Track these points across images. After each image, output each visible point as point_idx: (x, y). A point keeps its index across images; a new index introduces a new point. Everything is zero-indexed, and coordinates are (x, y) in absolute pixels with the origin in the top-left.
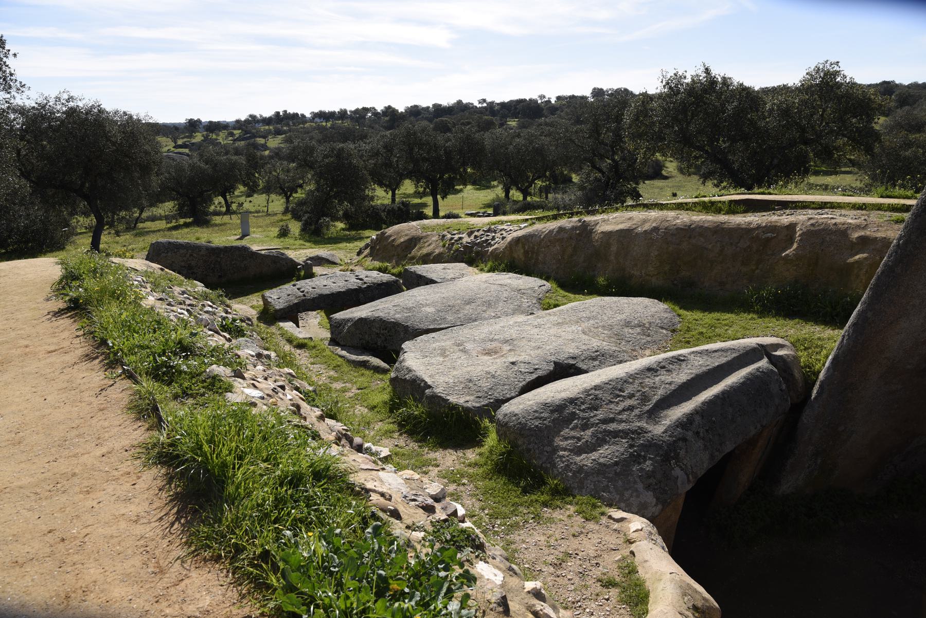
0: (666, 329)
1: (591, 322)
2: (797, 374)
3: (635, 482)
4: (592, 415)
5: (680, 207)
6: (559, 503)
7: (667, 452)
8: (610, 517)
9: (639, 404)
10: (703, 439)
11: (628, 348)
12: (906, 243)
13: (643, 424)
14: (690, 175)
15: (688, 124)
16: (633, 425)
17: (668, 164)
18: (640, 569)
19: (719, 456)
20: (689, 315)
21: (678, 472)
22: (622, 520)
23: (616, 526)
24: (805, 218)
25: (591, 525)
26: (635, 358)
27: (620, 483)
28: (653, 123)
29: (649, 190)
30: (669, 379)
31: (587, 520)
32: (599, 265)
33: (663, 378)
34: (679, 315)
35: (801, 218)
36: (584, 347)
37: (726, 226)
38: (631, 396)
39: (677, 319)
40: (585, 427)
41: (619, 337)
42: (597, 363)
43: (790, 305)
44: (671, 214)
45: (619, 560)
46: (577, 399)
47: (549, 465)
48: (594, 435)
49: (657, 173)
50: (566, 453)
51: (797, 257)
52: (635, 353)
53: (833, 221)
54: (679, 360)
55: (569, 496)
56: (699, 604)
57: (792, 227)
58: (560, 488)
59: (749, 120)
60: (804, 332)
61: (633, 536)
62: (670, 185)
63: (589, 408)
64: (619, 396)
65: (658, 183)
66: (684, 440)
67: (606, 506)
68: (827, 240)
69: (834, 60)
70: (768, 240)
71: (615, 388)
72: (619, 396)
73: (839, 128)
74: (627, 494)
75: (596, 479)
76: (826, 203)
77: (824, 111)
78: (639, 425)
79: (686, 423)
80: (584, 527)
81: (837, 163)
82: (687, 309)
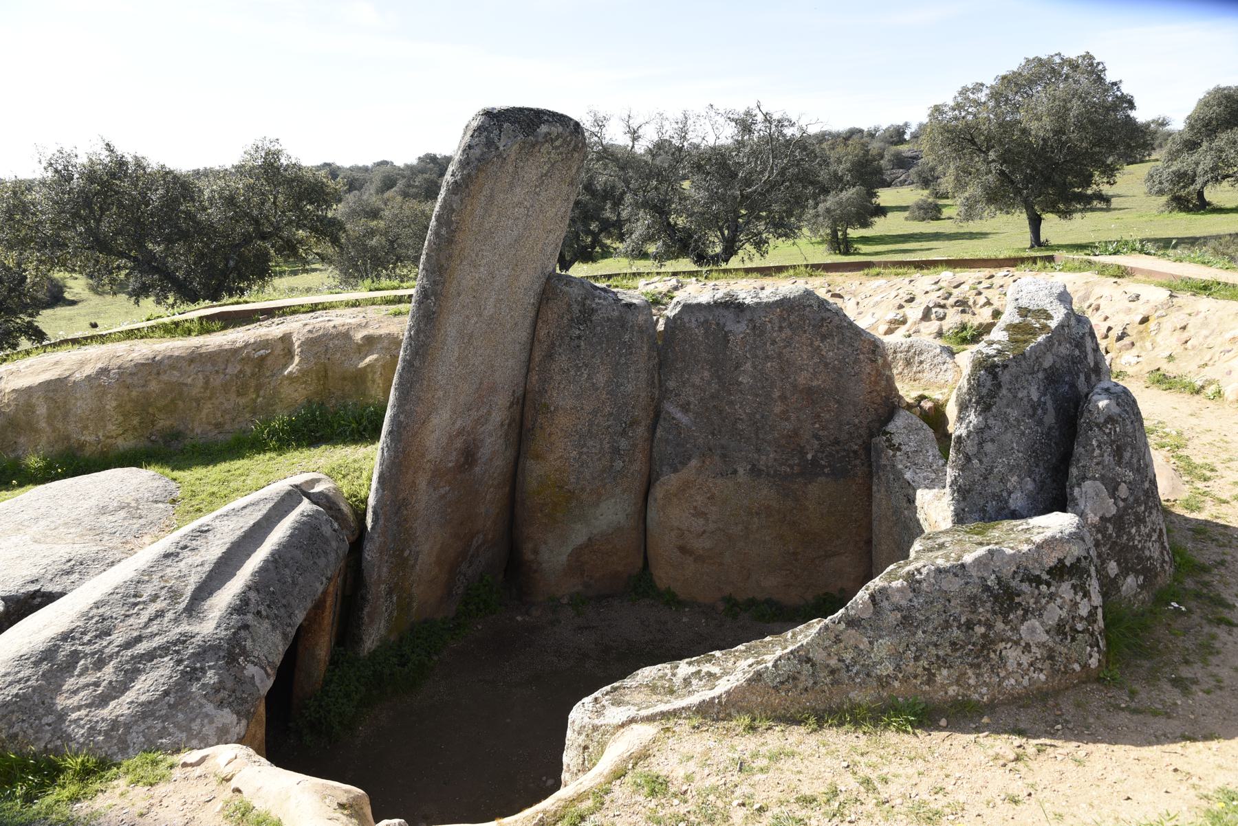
0: (163, 502)
1: (42, 523)
2: (345, 509)
3: (201, 706)
4: (105, 643)
5: (130, 334)
6: (97, 786)
7: (230, 651)
8: (185, 765)
9: (169, 604)
10: (267, 617)
11: (116, 541)
12: (417, 332)
13: (185, 627)
14: (115, 294)
15: (98, 221)
16: (171, 634)
17: (70, 283)
18: (255, 803)
19: (292, 632)
20: (187, 476)
21: (251, 670)
22: (202, 760)
23: (199, 770)
24: (299, 324)
25: (161, 789)
26: (132, 552)
27: (180, 716)
28: (40, 222)
29: (50, 321)
30: (197, 559)
31: (151, 785)
32: (22, 440)
33: (189, 561)
34: (175, 480)
35: (296, 326)
36: (45, 561)
37: (203, 351)
38: (154, 598)
39: (173, 485)
40: (100, 664)
41: (97, 532)
42: (75, 576)
43: (313, 429)
44: (121, 347)
45: (223, 809)
46: (72, 631)
47: (59, 743)
48: (117, 669)
49: (57, 298)
50: (83, 712)
51: (304, 373)
52: (128, 546)
53: (332, 324)
54: (203, 532)
55: (109, 768)
56: (344, 800)
57: (286, 339)
58: (90, 765)
59: (183, 212)
60: (335, 458)
61: (226, 771)
62: (83, 311)
63: (96, 637)
64: (136, 604)
65: (61, 311)
66: (246, 627)
67: (172, 754)
68: (326, 347)
69: (274, 137)
70: (263, 359)
71: (128, 596)
72: (136, 604)
73: (298, 217)
74: (195, 726)
75: (143, 726)
76: (316, 305)
77: (275, 198)
78: (178, 630)
79: (241, 606)
80: (152, 797)
81: (305, 262)
82: (180, 469)
